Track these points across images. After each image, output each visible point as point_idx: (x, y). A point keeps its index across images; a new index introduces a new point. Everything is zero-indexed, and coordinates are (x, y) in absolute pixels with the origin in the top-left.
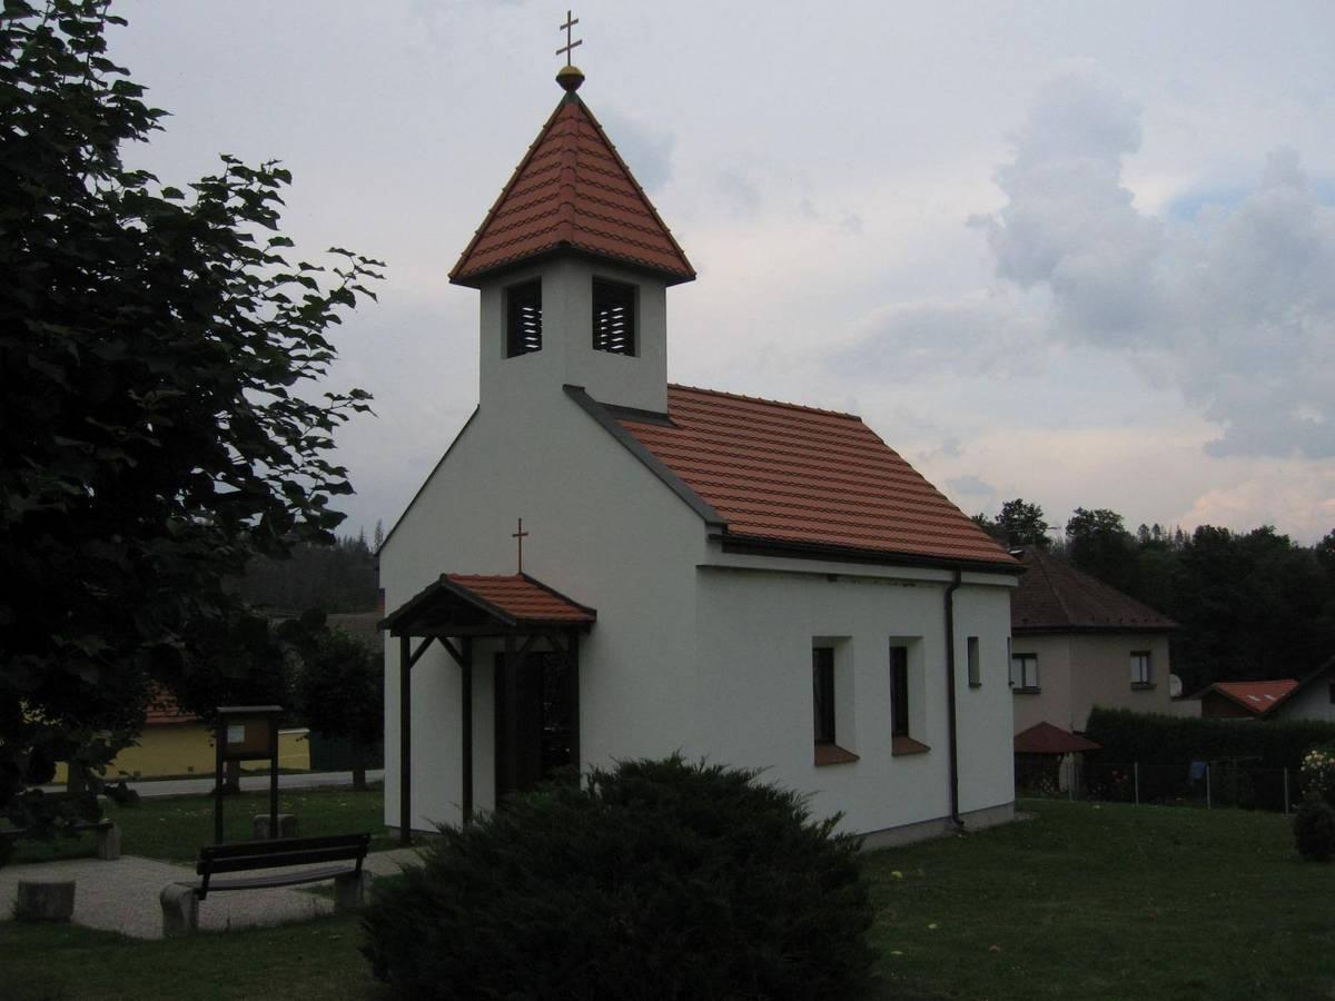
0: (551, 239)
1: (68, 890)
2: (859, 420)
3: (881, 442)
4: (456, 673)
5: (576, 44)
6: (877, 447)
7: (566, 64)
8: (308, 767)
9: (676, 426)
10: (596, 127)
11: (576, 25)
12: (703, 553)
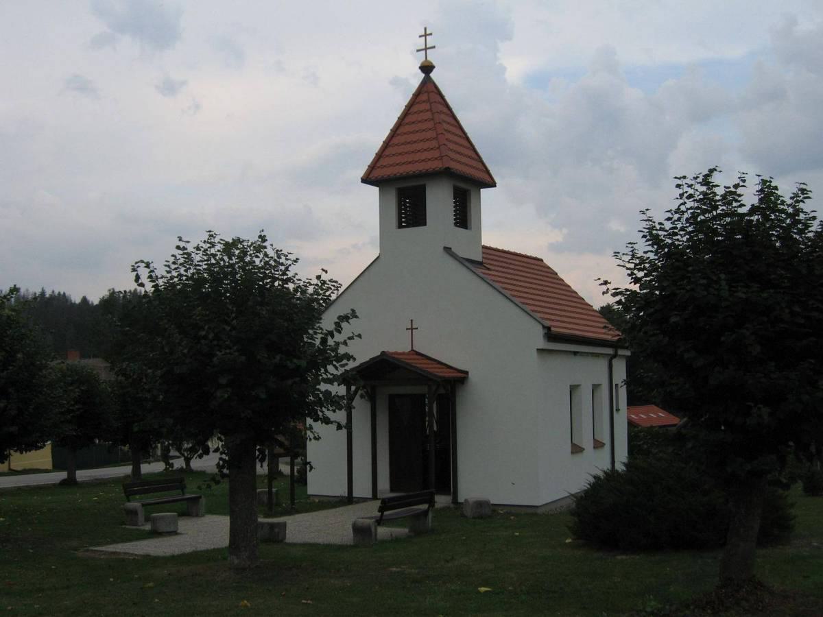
0: (437, 165)
1: (284, 525)
2: (542, 260)
3: (557, 274)
4: (368, 405)
5: (422, 50)
6: (553, 276)
7: (424, 59)
8: (49, 466)
9: (489, 269)
10: (442, 97)
11: (420, 34)
12: (541, 343)
